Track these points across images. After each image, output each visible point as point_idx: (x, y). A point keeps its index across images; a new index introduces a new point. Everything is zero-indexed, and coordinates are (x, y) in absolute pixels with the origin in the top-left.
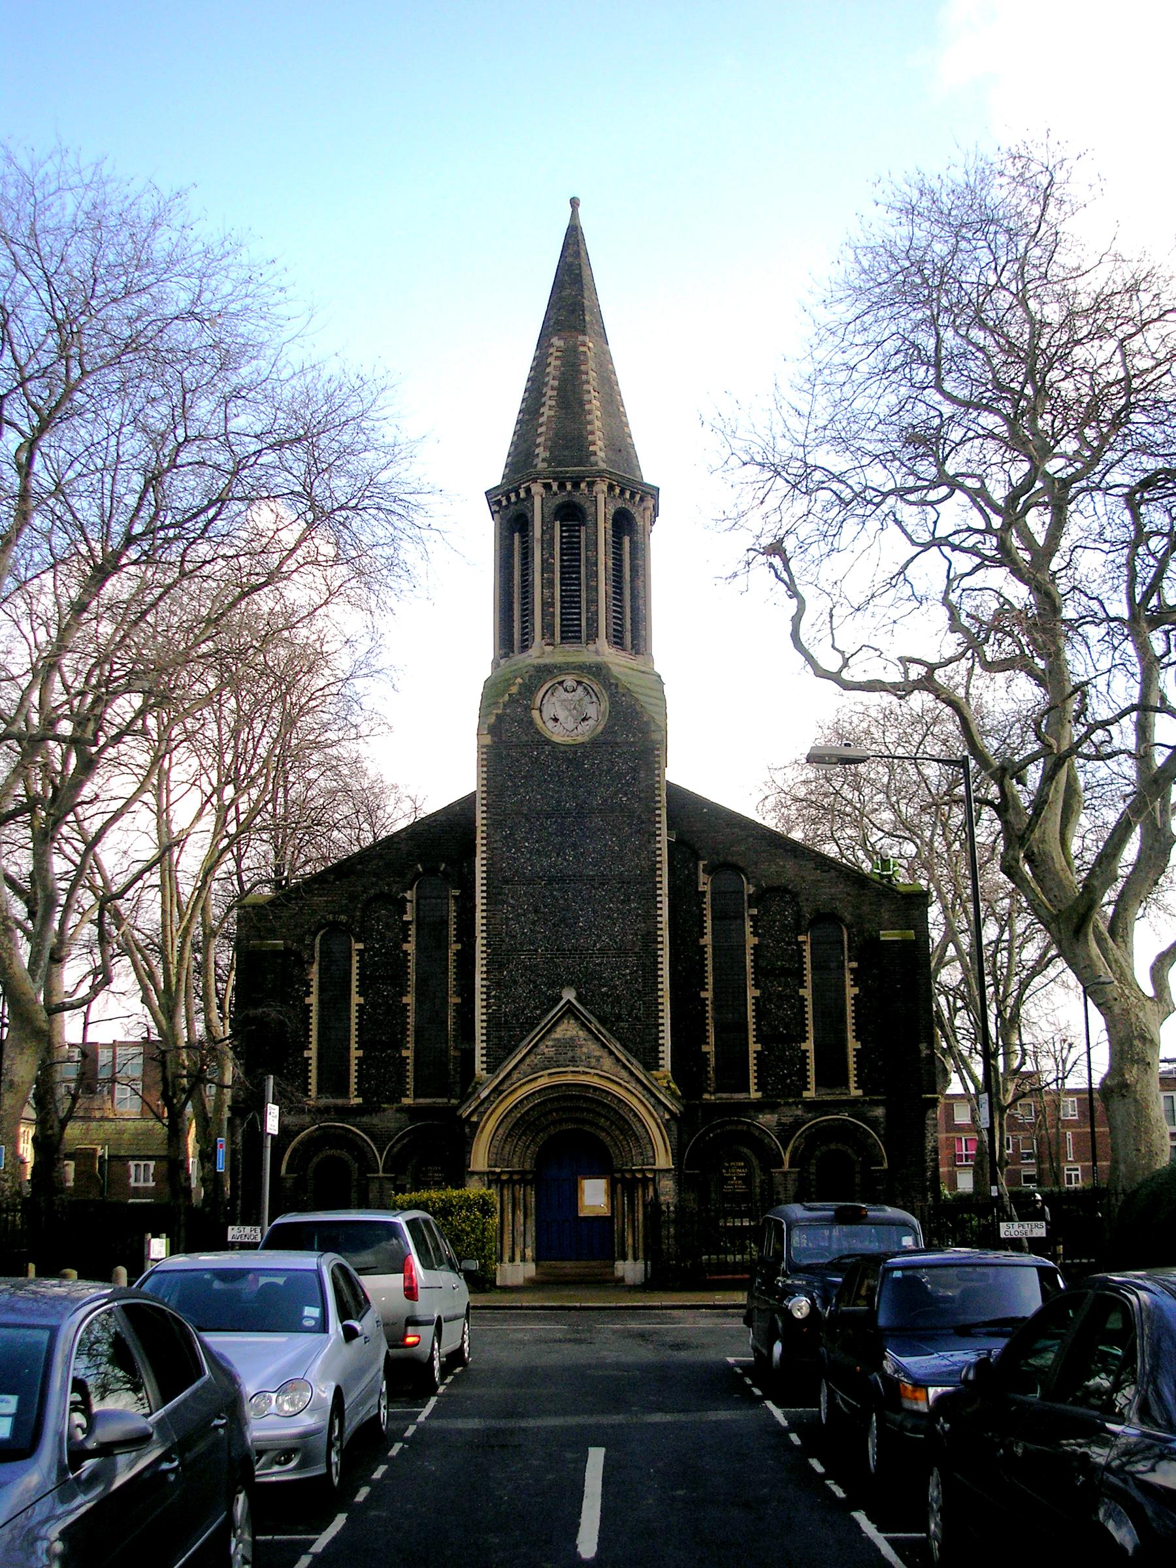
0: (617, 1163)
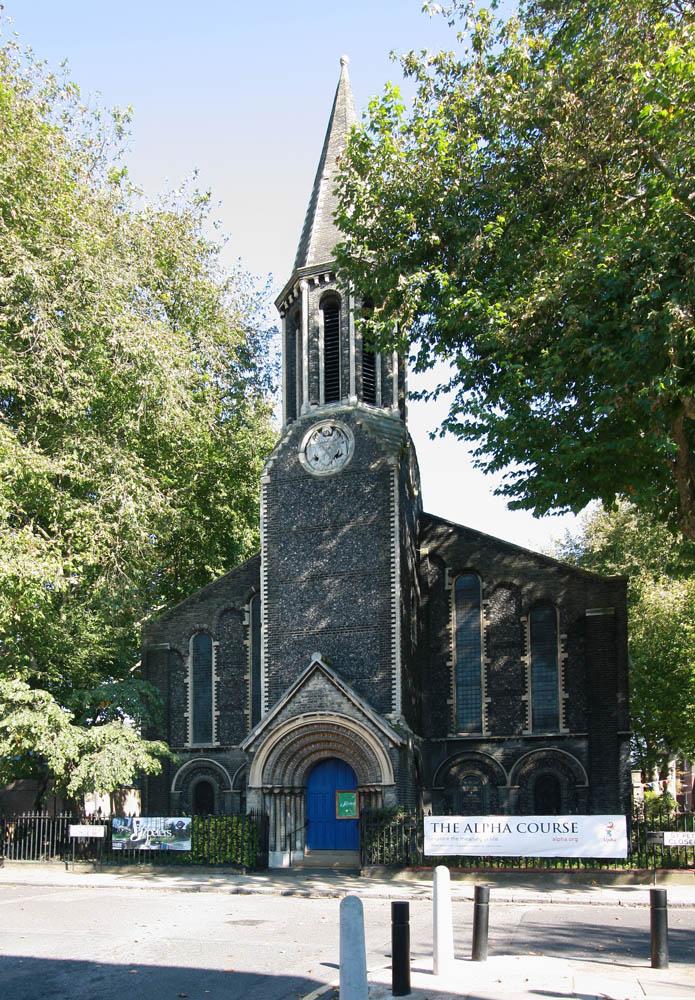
0: (361, 782)
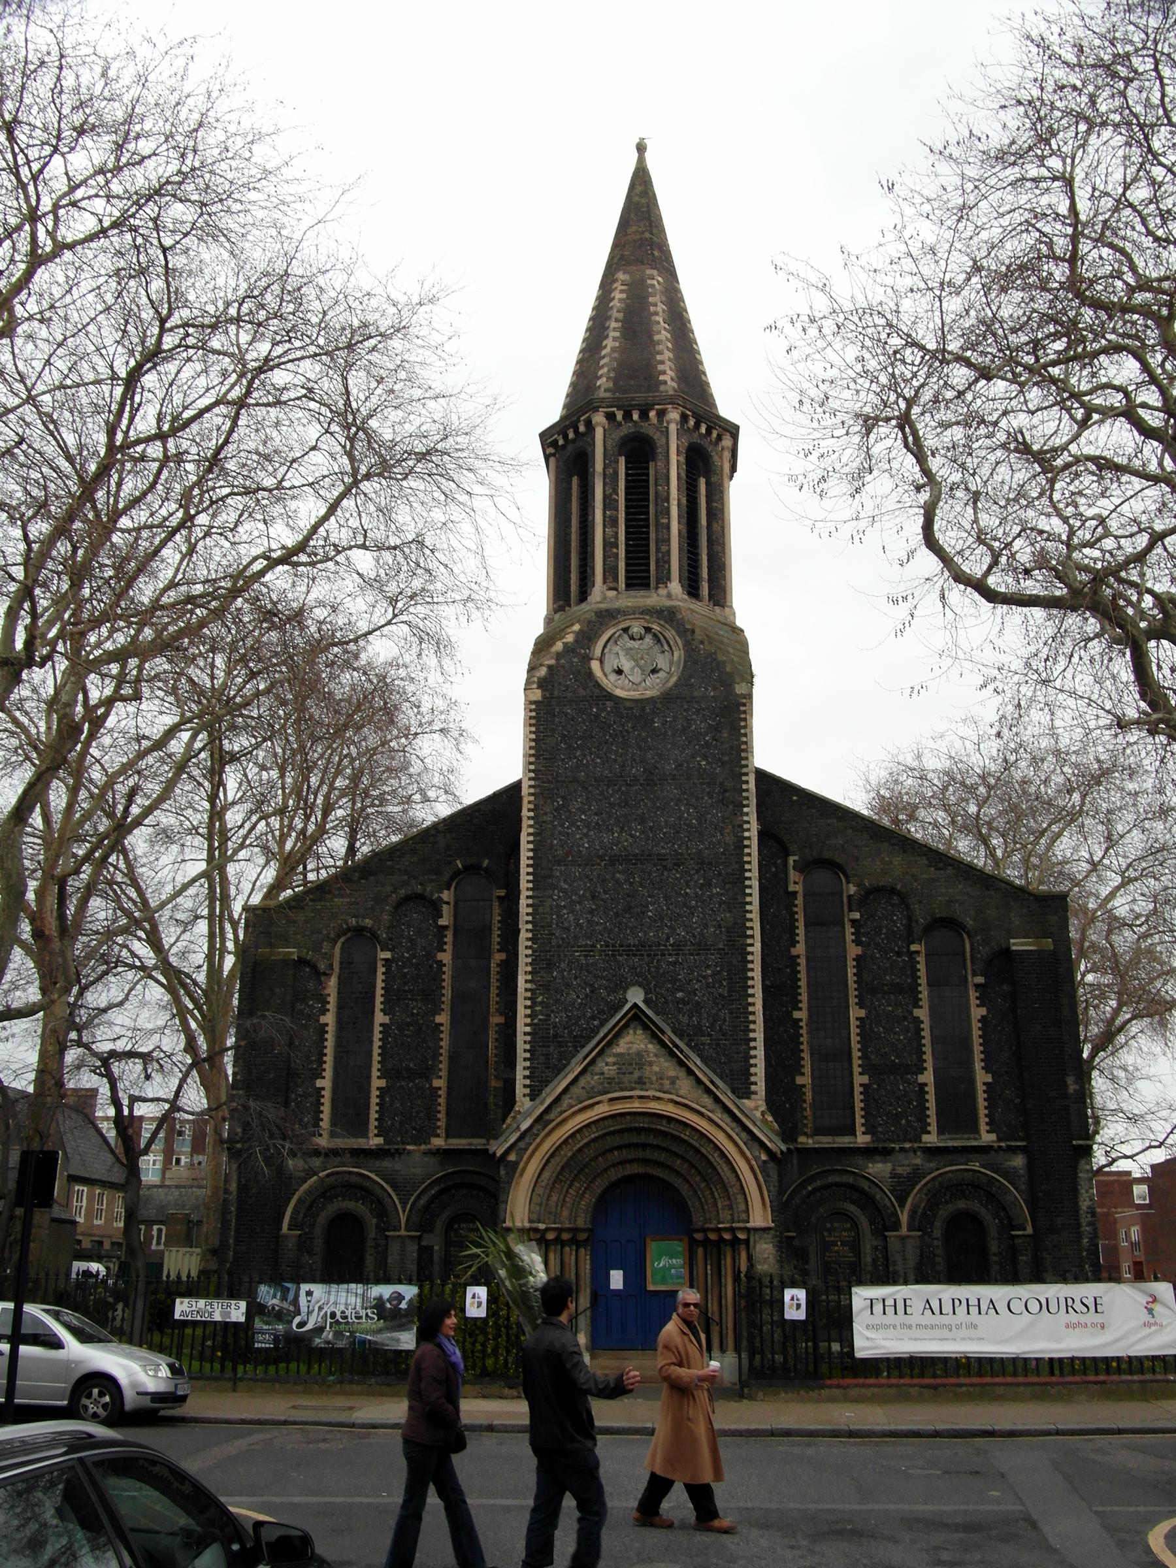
0: (698, 1220)
